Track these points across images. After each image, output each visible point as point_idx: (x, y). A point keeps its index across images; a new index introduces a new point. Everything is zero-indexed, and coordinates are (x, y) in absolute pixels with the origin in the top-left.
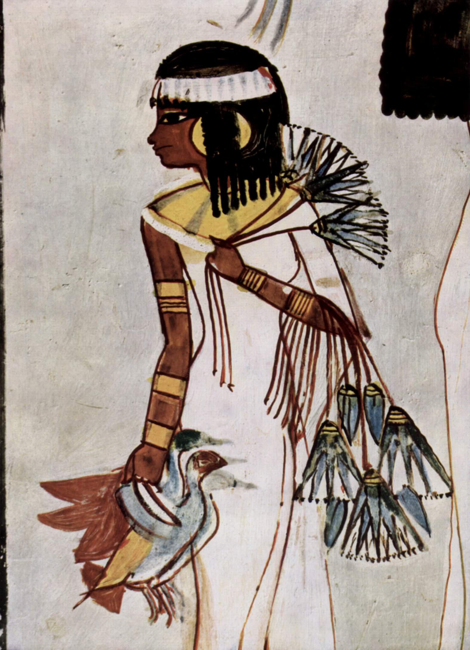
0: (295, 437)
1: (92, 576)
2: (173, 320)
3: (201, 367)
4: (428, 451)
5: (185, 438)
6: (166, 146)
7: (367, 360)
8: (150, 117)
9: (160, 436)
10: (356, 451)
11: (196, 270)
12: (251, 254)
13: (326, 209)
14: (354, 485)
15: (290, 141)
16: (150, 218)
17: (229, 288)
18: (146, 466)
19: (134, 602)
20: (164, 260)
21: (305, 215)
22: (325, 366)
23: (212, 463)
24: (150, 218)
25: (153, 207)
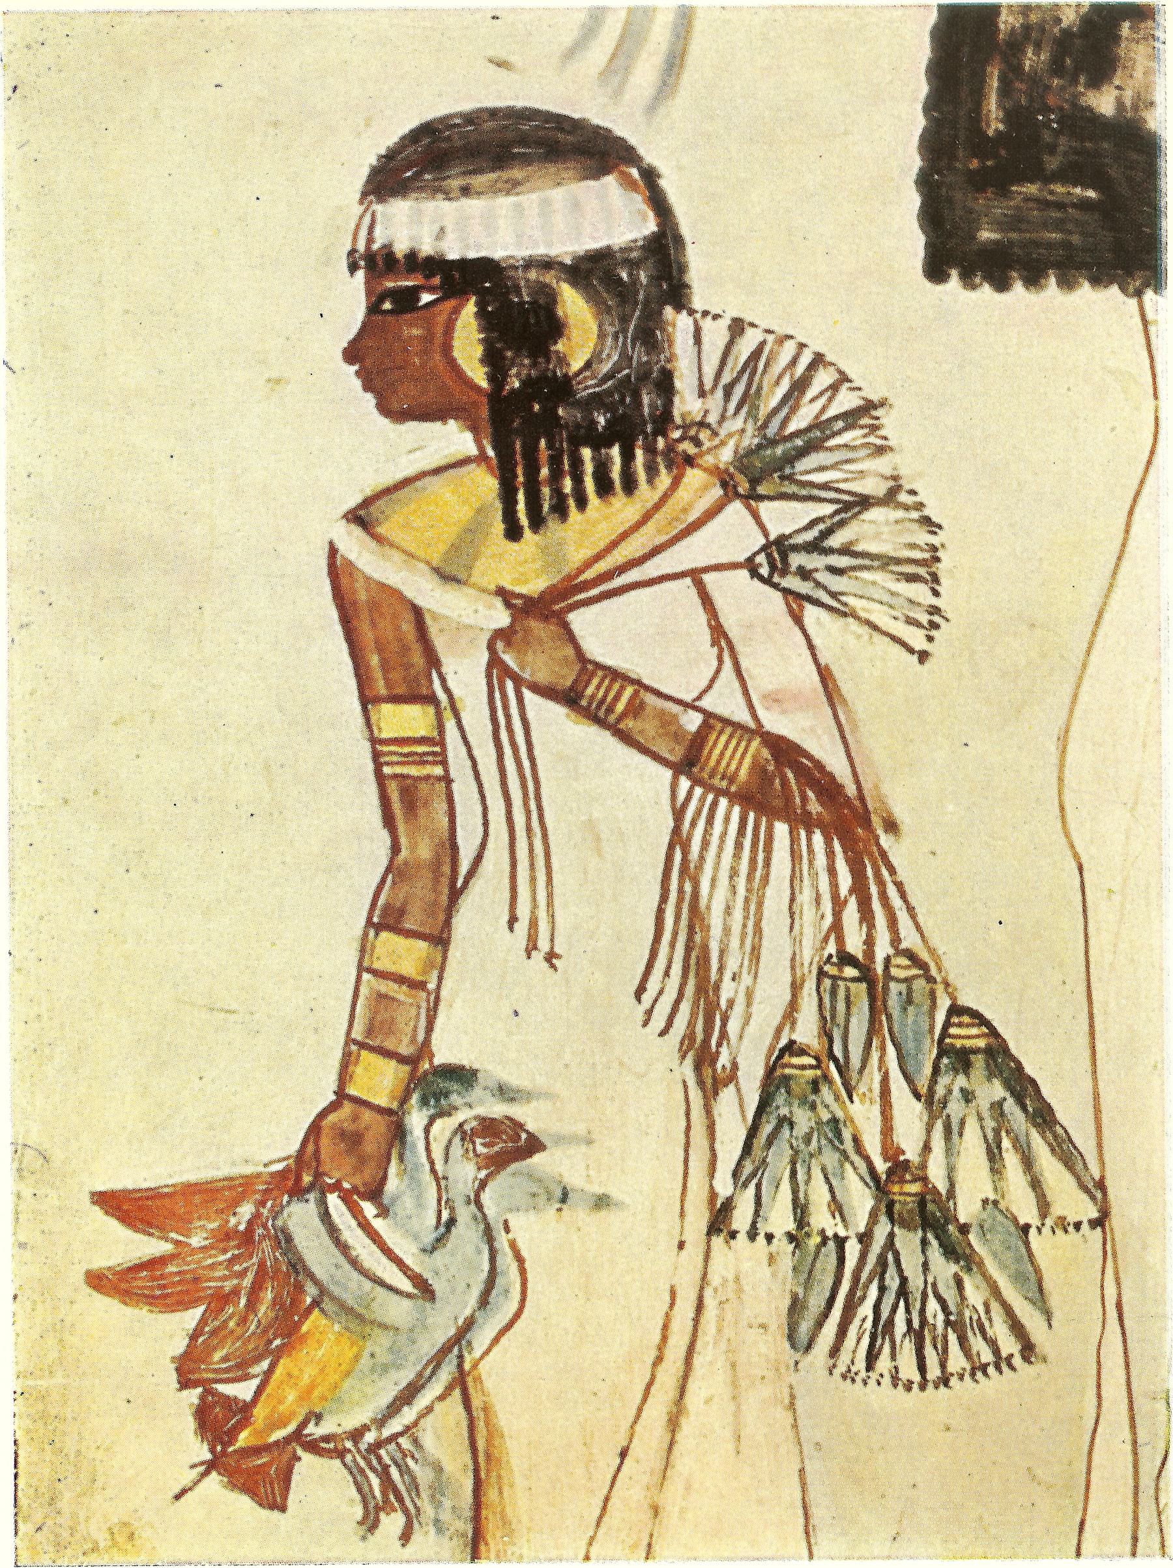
0: (708, 1070)
1: (217, 1421)
2: (406, 791)
3: (479, 916)
4: (1044, 1117)
6: (393, 367)
8: (349, 302)
9: (379, 1081)
10: (864, 1116)
11: (464, 674)
12: (600, 630)
13: (785, 517)
14: (861, 1200)
15: (691, 351)
16: (355, 546)
17: (547, 716)
18: (346, 1154)
19: (320, 1484)
20: (389, 651)
21: (734, 533)
22: (780, 918)
23: (508, 1145)
24: (355, 546)
25: (361, 517)
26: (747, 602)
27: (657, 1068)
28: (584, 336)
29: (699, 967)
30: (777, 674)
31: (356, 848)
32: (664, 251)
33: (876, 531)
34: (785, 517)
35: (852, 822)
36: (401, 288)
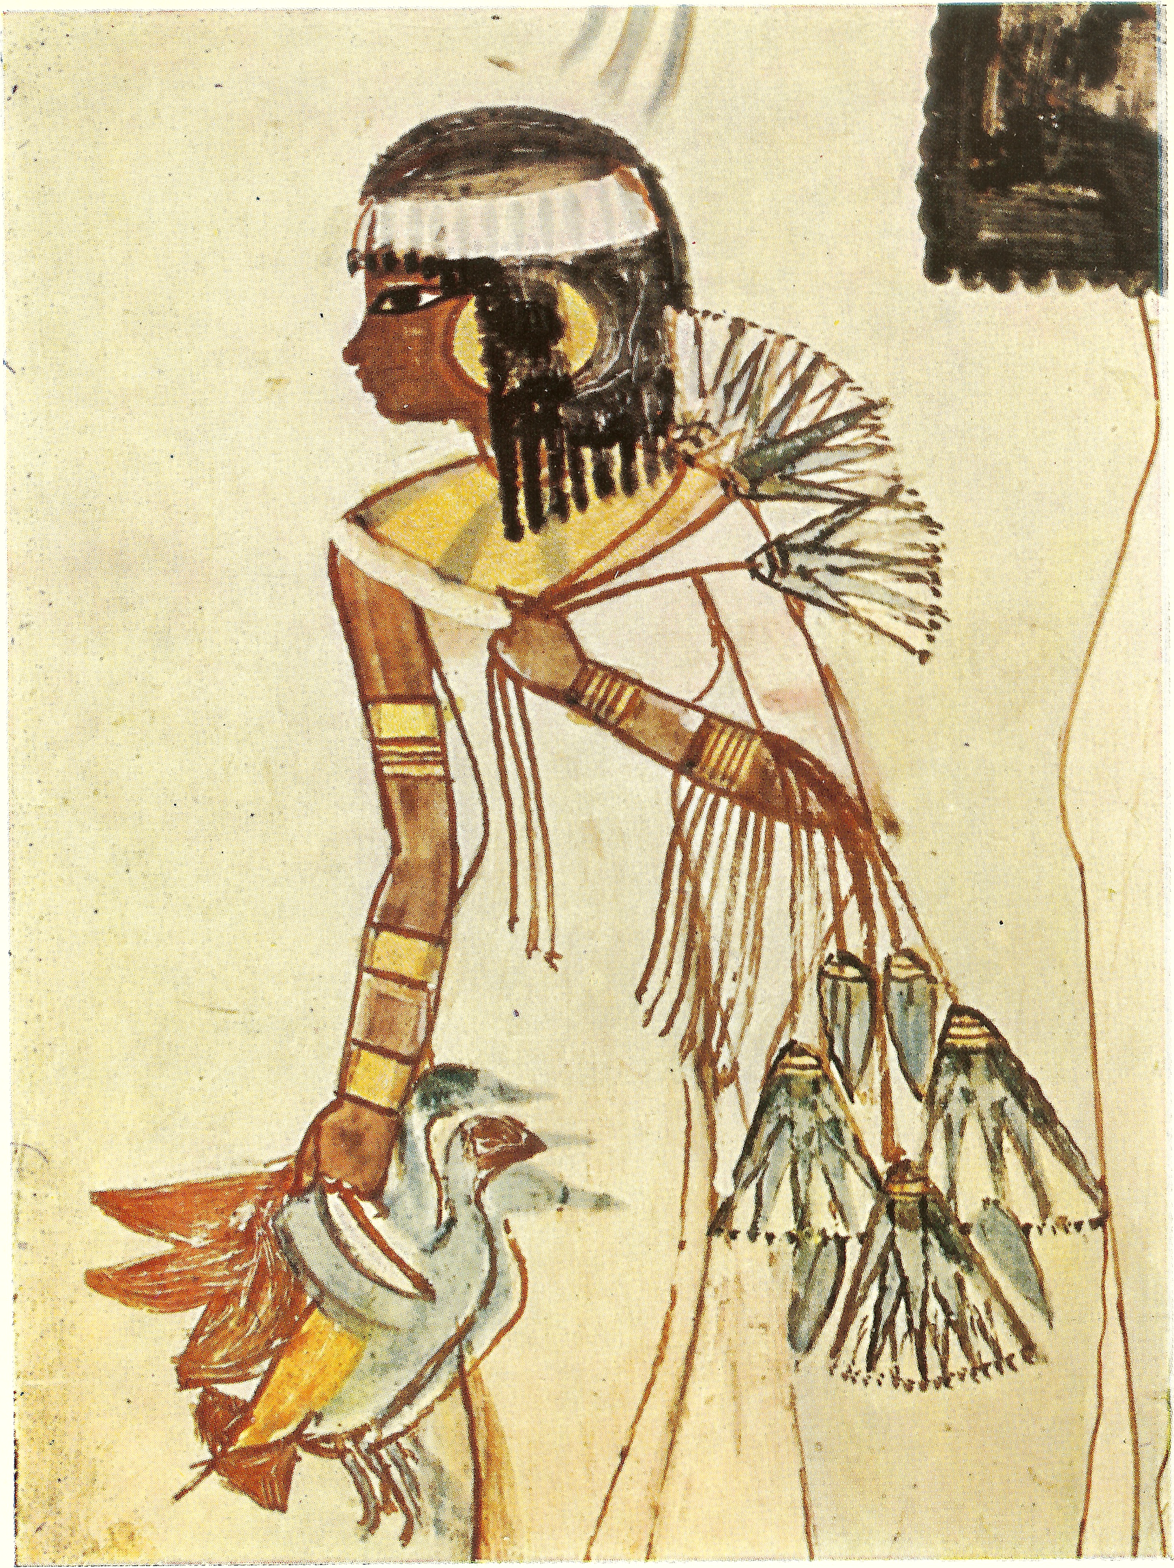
0: (709, 1070)
1: (217, 1421)
2: (406, 791)
3: (479, 916)
4: (1045, 1117)
5: (440, 1083)
6: (394, 367)
7: (893, 891)
8: (350, 301)
9: (379, 1081)
10: (865, 1116)
11: (465, 674)
12: (601, 630)
13: (786, 517)
14: (861, 1200)
15: (692, 351)
16: (355, 546)
17: (547, 716)
18: (347, 1154)
19: (320, 1484)
20: (389, 651)
21: (735, 533)
22: (780, 918)
23: (508, 1145)
24: (355, 546)
25: (361, 517)
26: (747, 602)
27: (657, 1069)
28: (585, 336)
29: (699, 966)
30: (777, 675)
31: (356, 848)
32: (665, 251)
33: (876, 531)
34: (786, 517)
35: (853, 822)
36: (402, 288)
